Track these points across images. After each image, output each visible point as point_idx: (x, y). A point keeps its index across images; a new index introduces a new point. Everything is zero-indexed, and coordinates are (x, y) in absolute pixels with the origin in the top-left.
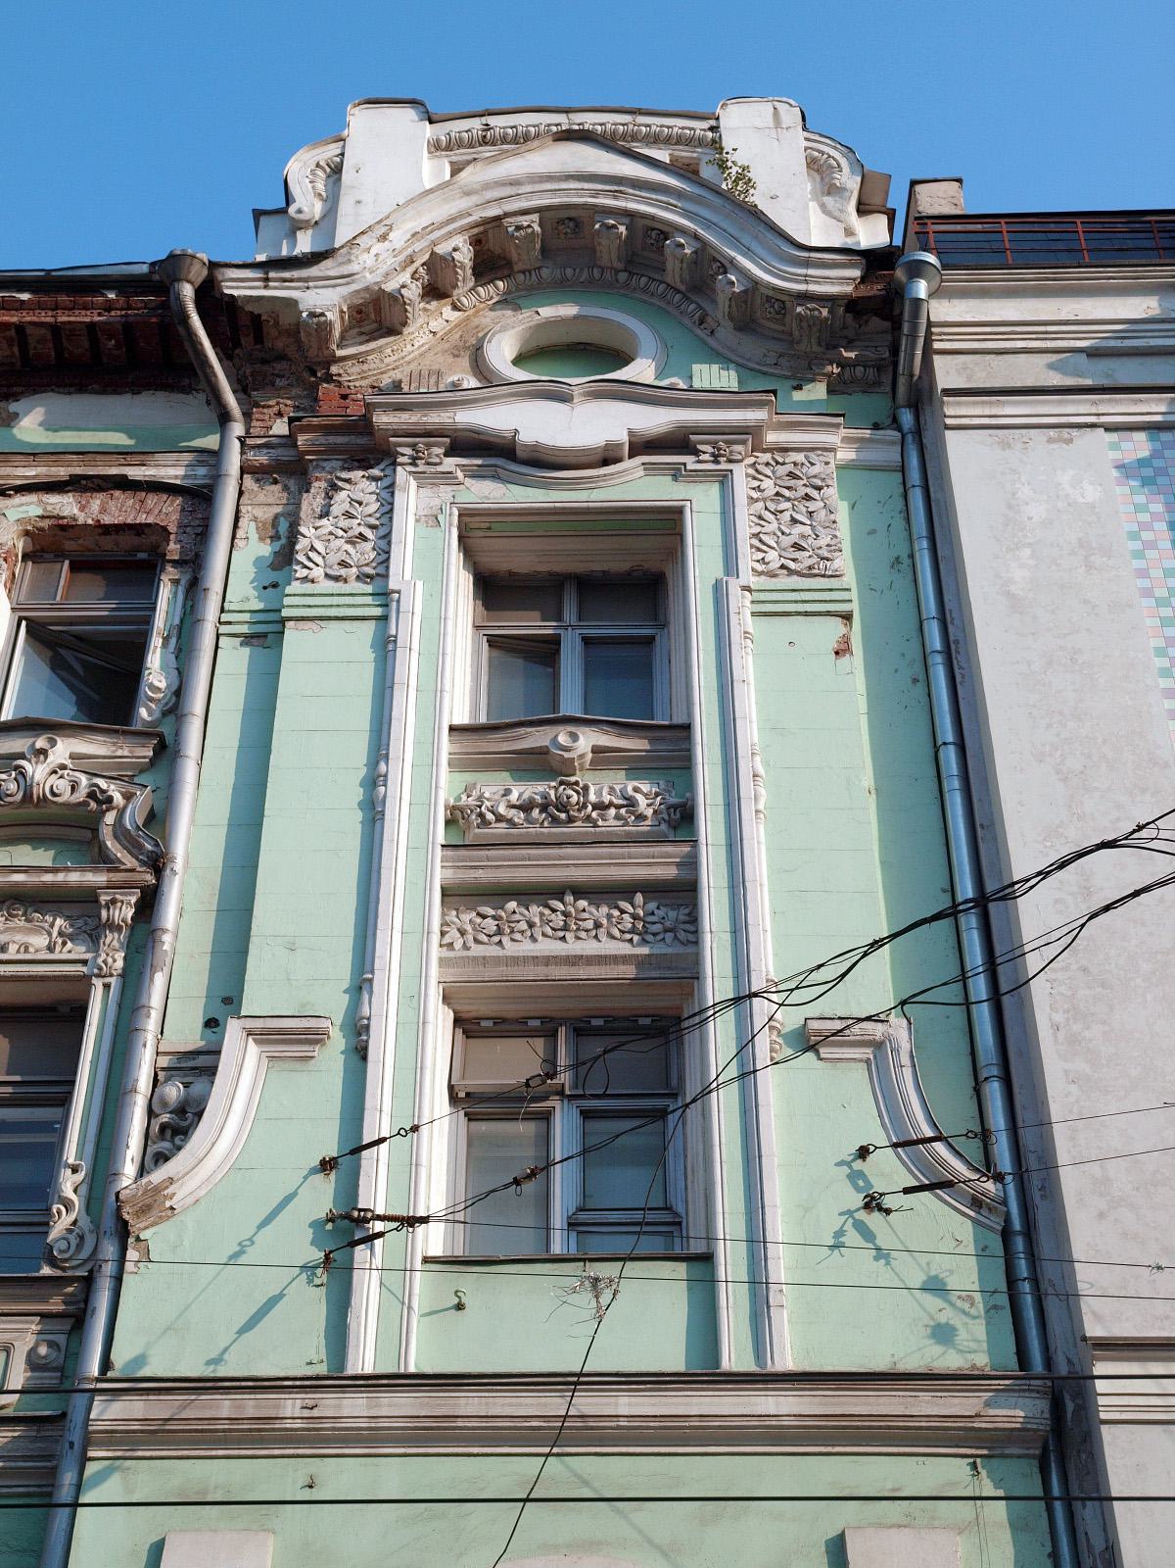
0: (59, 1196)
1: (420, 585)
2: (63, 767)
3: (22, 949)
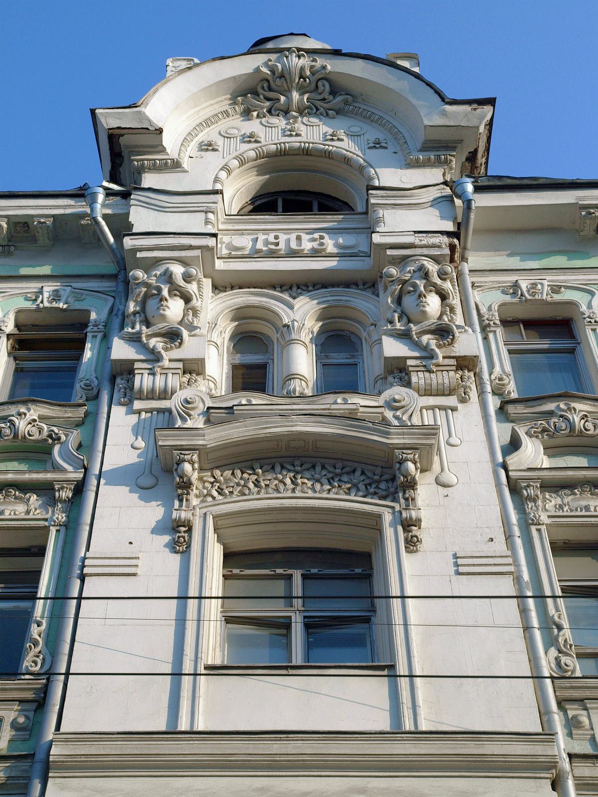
0: (31, 638)
1: (145, 341)
2: (34, 420)
3: (12, 513)
